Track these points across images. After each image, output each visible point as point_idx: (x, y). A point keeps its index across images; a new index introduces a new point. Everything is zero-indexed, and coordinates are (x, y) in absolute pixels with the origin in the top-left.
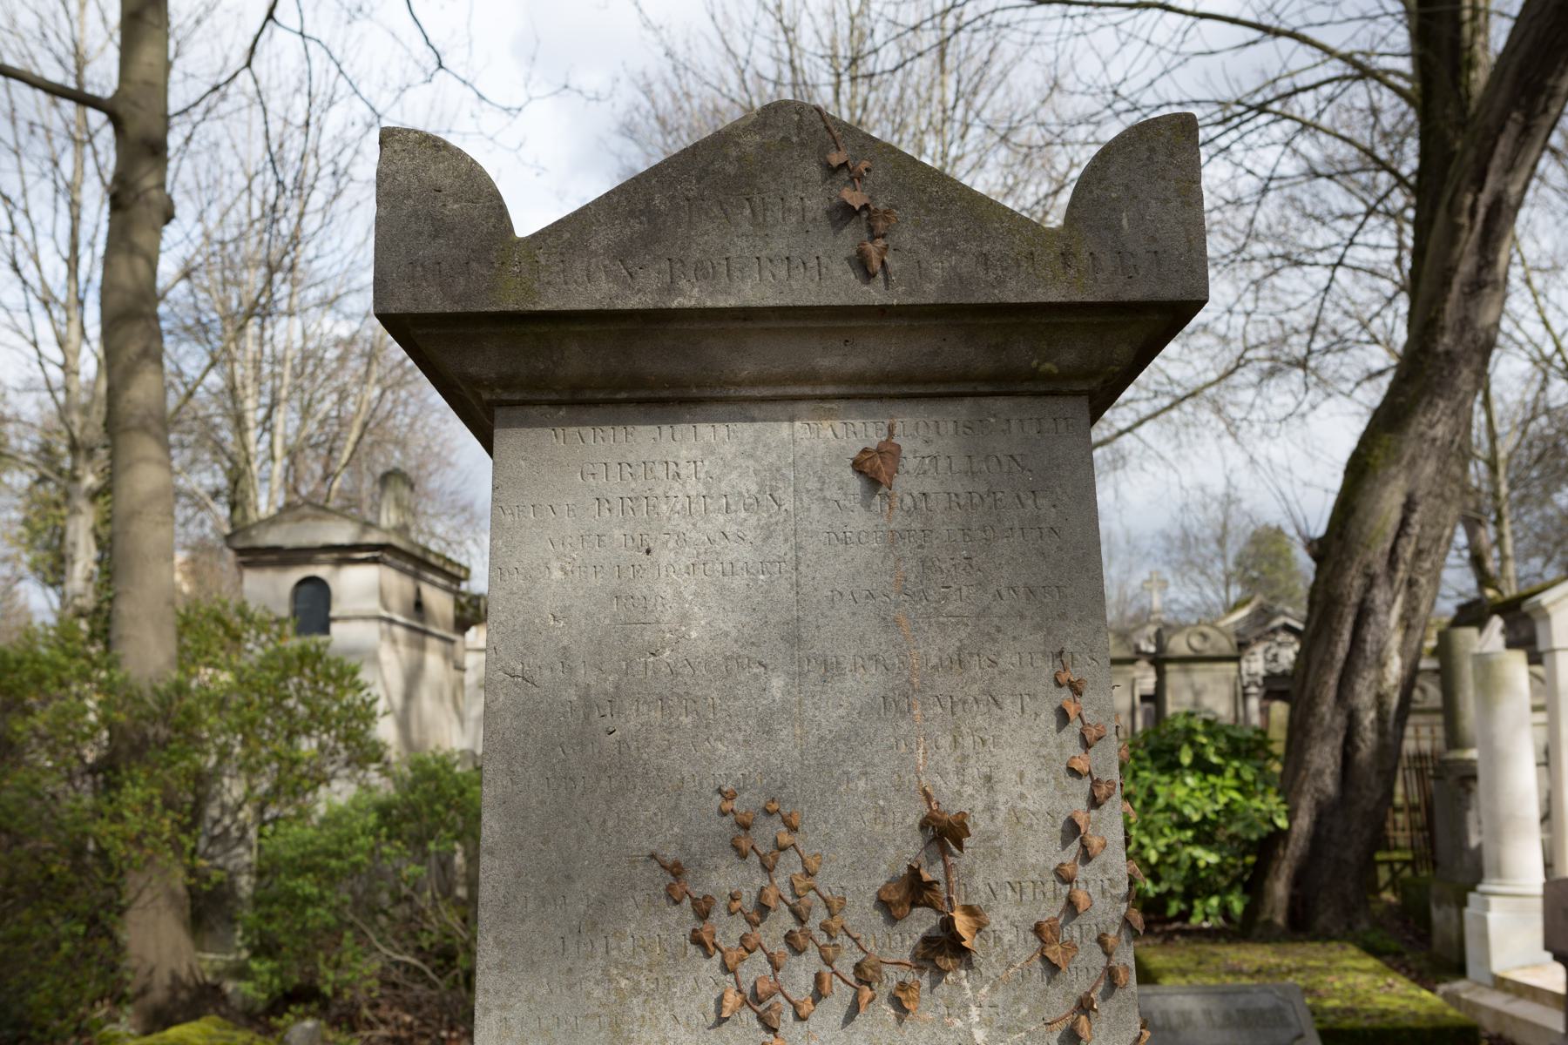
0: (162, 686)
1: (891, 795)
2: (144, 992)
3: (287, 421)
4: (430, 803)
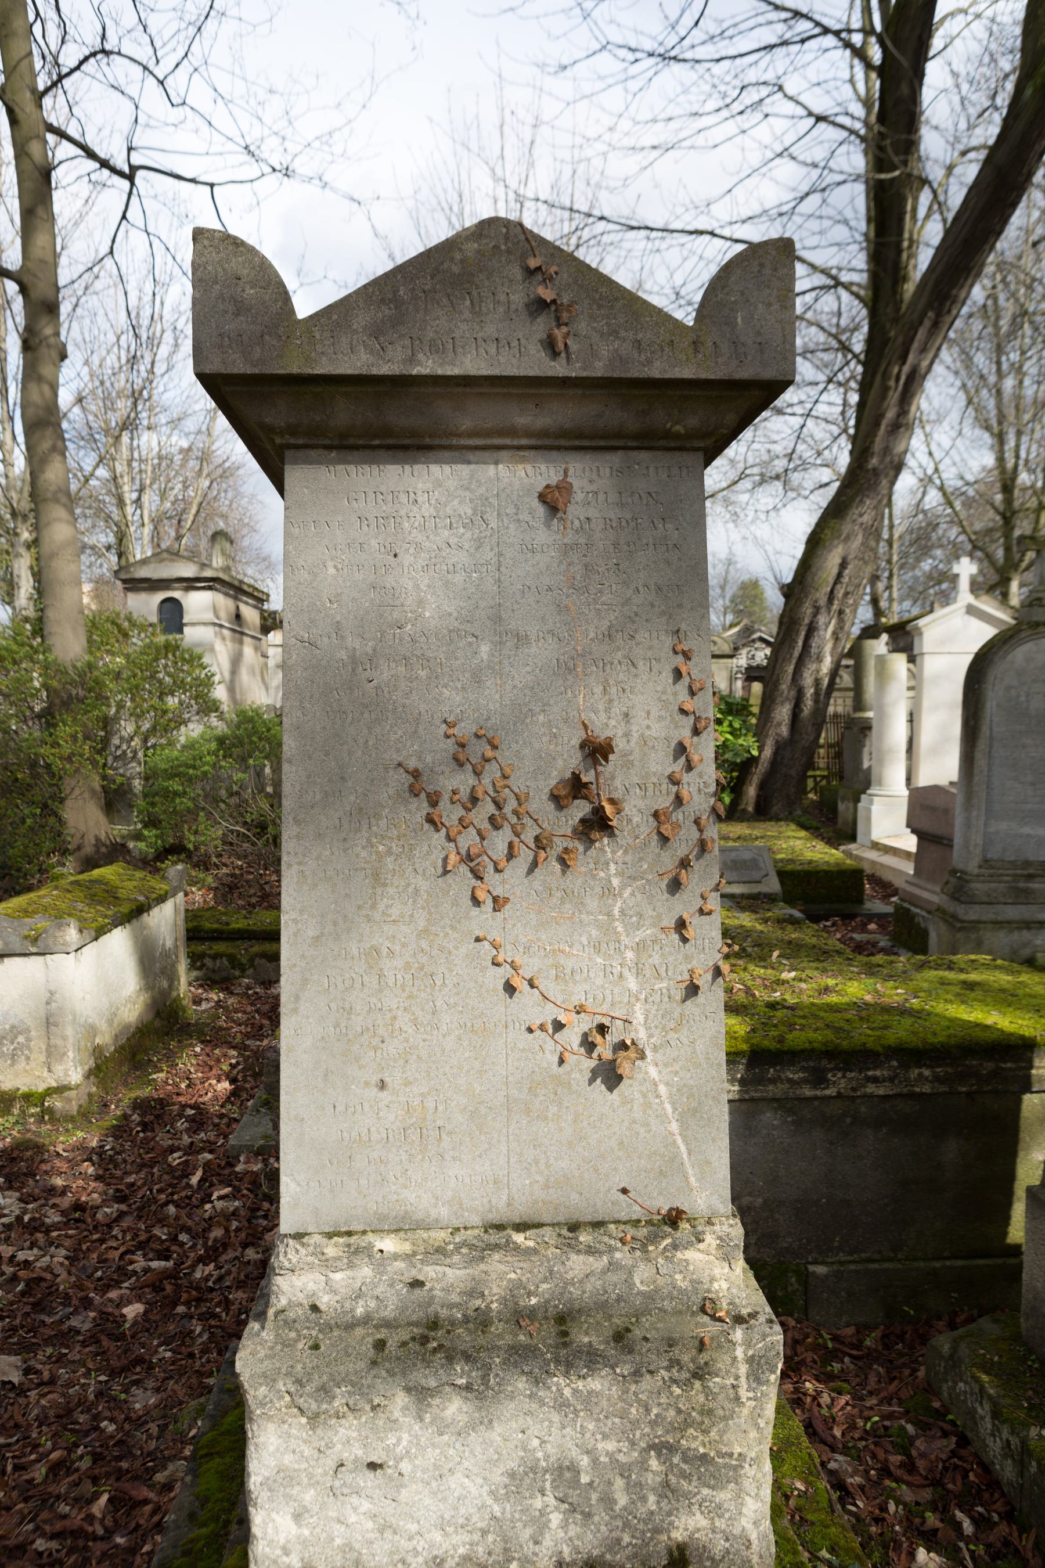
0: (79, 665)
1: (561, 725)
2: (79, 848)
3: (150, 499)
4: (249, 737)
